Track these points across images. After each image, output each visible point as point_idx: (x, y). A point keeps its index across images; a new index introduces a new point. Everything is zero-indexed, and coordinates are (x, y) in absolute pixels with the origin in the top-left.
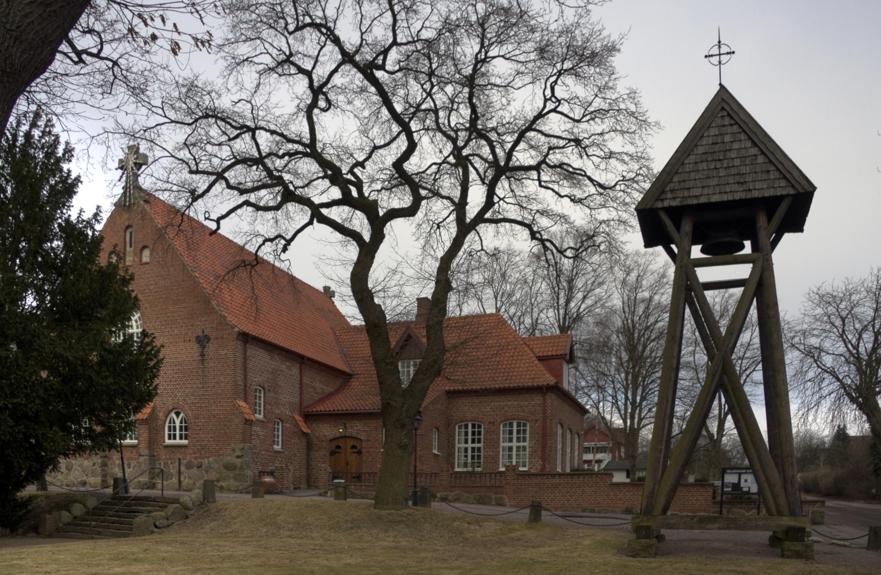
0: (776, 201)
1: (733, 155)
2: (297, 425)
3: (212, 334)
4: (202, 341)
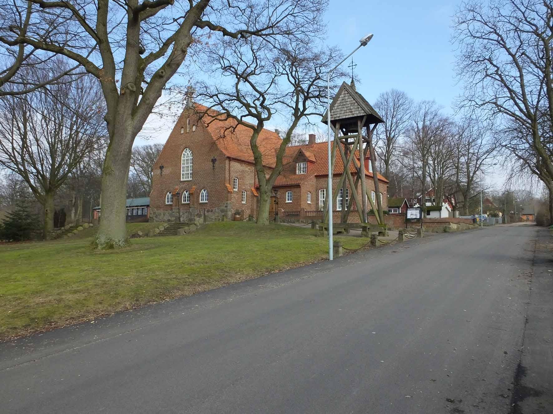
0: (362, 117)
1: (348, 103)
2: (252, 192)
3: (217, 158)
4: (214, 161)
